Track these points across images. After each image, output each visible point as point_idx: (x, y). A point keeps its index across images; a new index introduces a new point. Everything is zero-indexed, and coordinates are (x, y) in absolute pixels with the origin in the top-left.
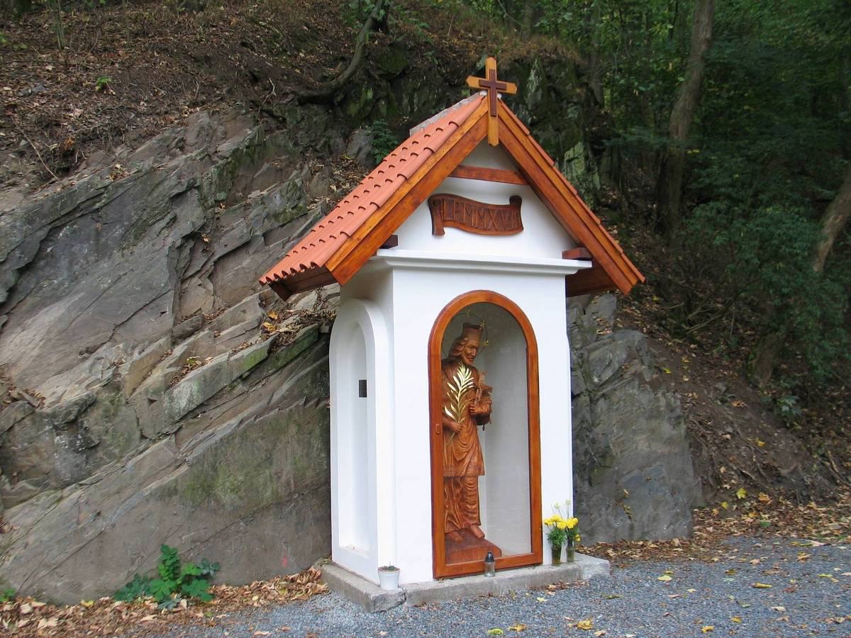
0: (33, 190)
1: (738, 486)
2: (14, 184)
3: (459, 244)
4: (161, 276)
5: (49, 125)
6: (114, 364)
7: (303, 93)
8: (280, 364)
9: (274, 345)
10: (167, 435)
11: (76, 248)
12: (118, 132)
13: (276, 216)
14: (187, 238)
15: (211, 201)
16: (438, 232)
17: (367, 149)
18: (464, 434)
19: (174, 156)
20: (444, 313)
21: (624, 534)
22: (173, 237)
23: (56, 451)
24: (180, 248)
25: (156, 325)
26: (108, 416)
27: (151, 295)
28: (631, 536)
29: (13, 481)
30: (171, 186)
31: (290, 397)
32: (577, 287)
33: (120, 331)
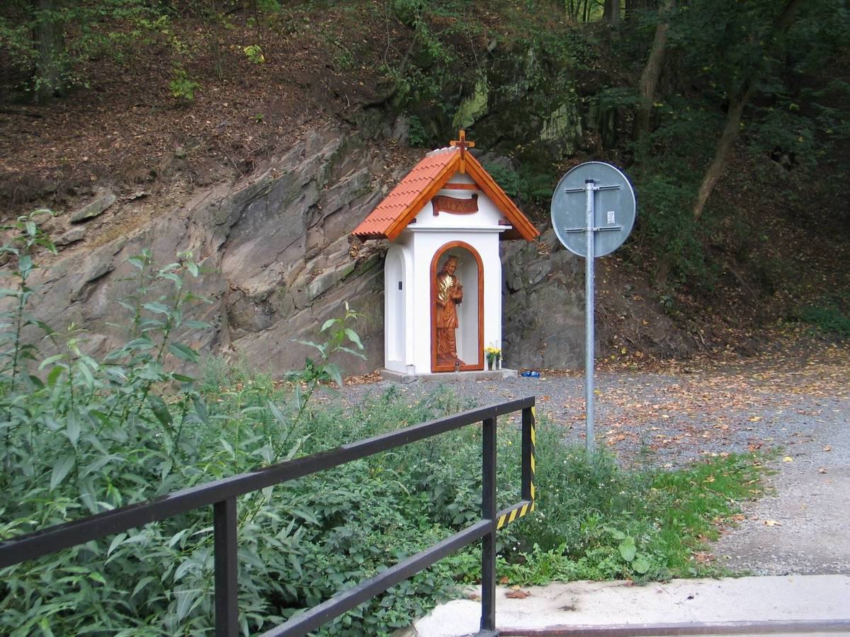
0: (233, 185)
1: (623, 346)
2: (224, 182)
3: (447, 219)
4: (300, 228)
5: (237, 147)
6: (280, 273)
7: (366, 103)
8: (360, 273)
9: (357, 263)
10: (307, 307)
11: (256, 214)
12: (272, 148)
13: (355, 192)
14: (310, 207)
15: (321, 185)
16: (436, 214)
17: (406, 135)
18: (448, 308)
19: (301, 161)
20: (438, 252)
21: (539, 365)
22: (303, 208)
23: (256, 315)
24: (307, 213)
25: (296, 253)
26: (280, 298)
27: (294, 238)
28: (543, 366)
29: (235, 328)
30: (302, 180)
31: (365, 289)
32: (503, 236)
33: (279, 256)
